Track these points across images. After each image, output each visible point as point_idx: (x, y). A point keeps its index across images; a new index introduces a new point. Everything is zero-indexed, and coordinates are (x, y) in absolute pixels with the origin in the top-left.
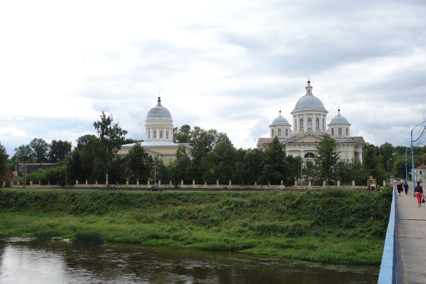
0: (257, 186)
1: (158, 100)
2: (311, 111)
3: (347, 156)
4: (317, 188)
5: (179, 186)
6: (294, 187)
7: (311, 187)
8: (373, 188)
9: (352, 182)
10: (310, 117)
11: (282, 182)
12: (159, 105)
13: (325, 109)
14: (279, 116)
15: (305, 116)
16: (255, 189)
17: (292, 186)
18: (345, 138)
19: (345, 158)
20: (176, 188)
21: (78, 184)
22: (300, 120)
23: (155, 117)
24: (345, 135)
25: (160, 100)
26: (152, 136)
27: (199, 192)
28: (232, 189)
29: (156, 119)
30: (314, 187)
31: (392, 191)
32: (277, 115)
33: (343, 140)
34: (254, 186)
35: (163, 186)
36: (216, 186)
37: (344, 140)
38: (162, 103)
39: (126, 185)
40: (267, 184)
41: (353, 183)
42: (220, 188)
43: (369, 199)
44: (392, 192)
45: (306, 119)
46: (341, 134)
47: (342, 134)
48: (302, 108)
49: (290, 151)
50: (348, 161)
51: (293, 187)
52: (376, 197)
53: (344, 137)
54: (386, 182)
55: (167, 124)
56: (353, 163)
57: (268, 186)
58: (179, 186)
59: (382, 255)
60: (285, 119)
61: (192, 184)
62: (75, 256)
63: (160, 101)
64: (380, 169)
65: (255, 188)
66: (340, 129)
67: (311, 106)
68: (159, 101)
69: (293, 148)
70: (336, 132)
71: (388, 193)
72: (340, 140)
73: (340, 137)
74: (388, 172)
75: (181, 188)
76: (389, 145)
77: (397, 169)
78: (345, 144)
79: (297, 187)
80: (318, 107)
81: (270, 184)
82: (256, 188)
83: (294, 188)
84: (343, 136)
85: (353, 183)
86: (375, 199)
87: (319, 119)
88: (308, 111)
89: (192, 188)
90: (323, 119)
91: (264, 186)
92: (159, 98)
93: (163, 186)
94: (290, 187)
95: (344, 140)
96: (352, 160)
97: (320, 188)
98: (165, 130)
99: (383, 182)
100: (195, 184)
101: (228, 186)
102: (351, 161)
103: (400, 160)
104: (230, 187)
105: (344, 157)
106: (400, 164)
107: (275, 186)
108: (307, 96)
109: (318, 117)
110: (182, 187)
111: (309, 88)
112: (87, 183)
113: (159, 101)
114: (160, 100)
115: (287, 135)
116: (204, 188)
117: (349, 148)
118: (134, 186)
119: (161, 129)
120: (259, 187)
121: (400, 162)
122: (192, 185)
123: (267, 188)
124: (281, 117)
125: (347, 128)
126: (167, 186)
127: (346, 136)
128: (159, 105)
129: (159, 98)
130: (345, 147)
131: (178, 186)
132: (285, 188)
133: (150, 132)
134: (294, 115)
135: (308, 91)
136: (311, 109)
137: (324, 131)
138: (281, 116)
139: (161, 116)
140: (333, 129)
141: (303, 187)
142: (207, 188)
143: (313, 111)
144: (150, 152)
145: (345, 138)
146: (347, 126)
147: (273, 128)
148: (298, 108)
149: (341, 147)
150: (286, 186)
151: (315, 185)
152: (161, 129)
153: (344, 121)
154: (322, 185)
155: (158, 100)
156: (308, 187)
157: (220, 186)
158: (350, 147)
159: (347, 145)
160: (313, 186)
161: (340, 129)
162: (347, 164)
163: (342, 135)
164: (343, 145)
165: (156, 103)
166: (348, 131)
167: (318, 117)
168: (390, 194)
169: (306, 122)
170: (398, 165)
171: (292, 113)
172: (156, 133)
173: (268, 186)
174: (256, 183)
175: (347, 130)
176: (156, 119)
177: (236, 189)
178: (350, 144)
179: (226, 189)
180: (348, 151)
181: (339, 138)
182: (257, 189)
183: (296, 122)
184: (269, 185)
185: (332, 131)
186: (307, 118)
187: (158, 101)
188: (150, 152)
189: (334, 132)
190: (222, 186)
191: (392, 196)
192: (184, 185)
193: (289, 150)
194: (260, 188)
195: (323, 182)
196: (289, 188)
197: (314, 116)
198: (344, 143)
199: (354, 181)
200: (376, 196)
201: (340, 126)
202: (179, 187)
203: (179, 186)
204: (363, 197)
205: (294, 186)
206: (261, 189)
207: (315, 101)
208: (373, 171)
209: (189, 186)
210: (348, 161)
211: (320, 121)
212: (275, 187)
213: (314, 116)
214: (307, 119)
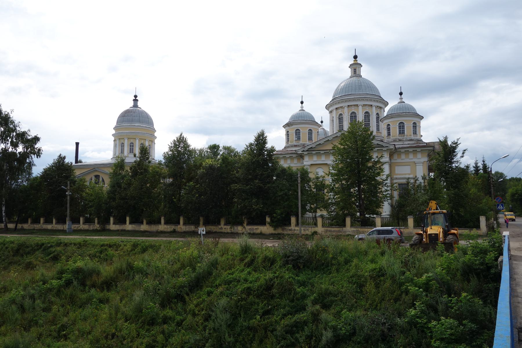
0: (225, 227)
1: (134, 98)
2: (354, 100)
3: (414, 170)
4: (334, 231)
5: (108, 227)
6: (291, 230)
7: (323, 229)
8: (434, 238)
9: (407, 220)
10: (353, 111)
11: (268, 219)
12: (135, 105)
13: (382, 98)
14: (300, 109)
15: (346, 109)
16: (221, 233)
17: (287, 228)
18: (411, 140)
19: (411, 176)
20: (104, 231)
21: (30, 224)
22: (338, 116)
23: (123, 122)
24: (410, 135)
25: (137, 98)
26: (128, 150)
27: (95, 240)
28: (185, 232)
29: (124, 125)
30: (329, 229)
31: (502, 254)
32: (296, 109)
33: (407, 144)
34: (220, 227)
35: (86, 227)
36: (160, 226)
37: (409, 144)
38: (139, 104)
39: (40, 225)
40: (241, 224)
41: (411, 221)
42: (166, 230)
43: (401, 284)
44: (496, 259)
45: (347, 114)
46: (404, 133)
47: (405, 133)
48: (341, 96)
49: (312, 165)
50: (416, 181)
51: (287, 231)
52: (428, 281)
53: (408, 139)
54: (487, 220)
55: (140, 132)
56: (426, 184)
57: (244, 227)
58: (108, 226)
59: (495, 325)
60: (308, 113)
61: (125, 223)
62: (427, 240)
63: (137, 100)
64: (473, 190)
65: (221, 231)
66: (401, 126)
67: (355, 92)
68: (136, 100)
69: (315, 160)
70: (395, 131)
71: (482, 264)
72: (402, 143)
73: (401, 138)
74: (493, 196)
75: (109, 230)
76: (500, 174)
77: (512, 201)
78: (411, 150)
79: (295, 230)
80: (368, 94)
81: (248, 224)
82: (223, 230)
83: (290, 232)
84: (407, 136)
85: (411, 221)
86: (427, 287)
87: (371, 114)
88: (350, 100)
89: (124, 230)
90: (377, 114)
91: (236, 228)
92: (136, 96)
93: (86, 226)
94: (283, 230)
95: (409, 144)
96: (424, 178)
97: (339, 231)
98: (137, 141)
99: (481, 219)
100: (130, 223)
101: (179, 226)
102: (422, 181)
103: (515, 188)
104: (181, 228)
105: (409, 174)
106: (516, 194)
107: (255, 227)
108: (353, 78)
109: (367, 109)
110: (112, 229)
111: (355, 66)
112: (181, 222)
113: (136, 100)
114: (137, 98)
115: (310, 139)
116: (142, 230)
117: (418, 158)
118: (49, 227)
119: (132, 141)
120: (227, 229)
121: (516, 191)
122: (125, 226)
123: (241, 232)
124: (304, 110)
125: (414, 123)
126: (91, 228)
127: (413, 137)
128: (135, 105)
129: (136, 96)
130: (411, 156)
131: (106, 226)
132: (274, 232)
133: (123, 143)
134: (330, 110)
135: (353, 71)
136: (356, 97)
137: (379, 134)
138: (304, 109)
139: (132, 121)
140: (389, 125)
141: (308, 230)
142: (146, 230)
143: (359, 99)
144: (102, 172)
145: (411, 140)
146: (415, 120)
147: (288, 128)
148: (336, 98)
149: (403, 156)
150: (275, 227)
151: (331, 225)
152: (132, 141)
153: (409, 110)
154: (345, 226)
155: (134, 98)
156: (316, 229)
157: (166, 226)
158: (419, 155)
159: (415, 152)
160: (326, 229)
161: (401, 126)
162: (415, 185)
163: (406, 134)
164: (407, 153)
165: (132, 104)
166: (417, 128)
167: (367, 109)
168: (489, 268)
169: (347, 119)
170: (513, 195)
171: (327, 107)
172: (123, 146)
173: (244, 227)
174: (222, 222)
175: (416, 127)
176: (124, 125)
177: (191, 232)
178: (419, 150)
179: (174, 231)
180: (416, 164)
181: (400, 140)
182: (225, 233)
183: (333, 121)
184: (245, 225)
185: (388, 128)
186: (348, 113)
187: (134, 100)
188: (102, 172)
189: (391, 131)
190: (168, 226)
191: (498, 278)
192: (114, 226)
193: (310, 163)
194: (229, 231)
195: (180, 218)
196: (279, 231)
197: (360, 107)
198: (408, 147)
199: (411, 216)
200: (430, 274)
201: (401, 119)
202: (108, 228)
203: (108, 227)
204: (383, 275)
205: (290, 228)
206: (232, 233)
207: (362, 84)
208: (453, 194)
209: (121, 226)
210: (416, 181)
211: (371, 116)
212: (256, 229)
213: (360, 107)
214: (349, 114)
